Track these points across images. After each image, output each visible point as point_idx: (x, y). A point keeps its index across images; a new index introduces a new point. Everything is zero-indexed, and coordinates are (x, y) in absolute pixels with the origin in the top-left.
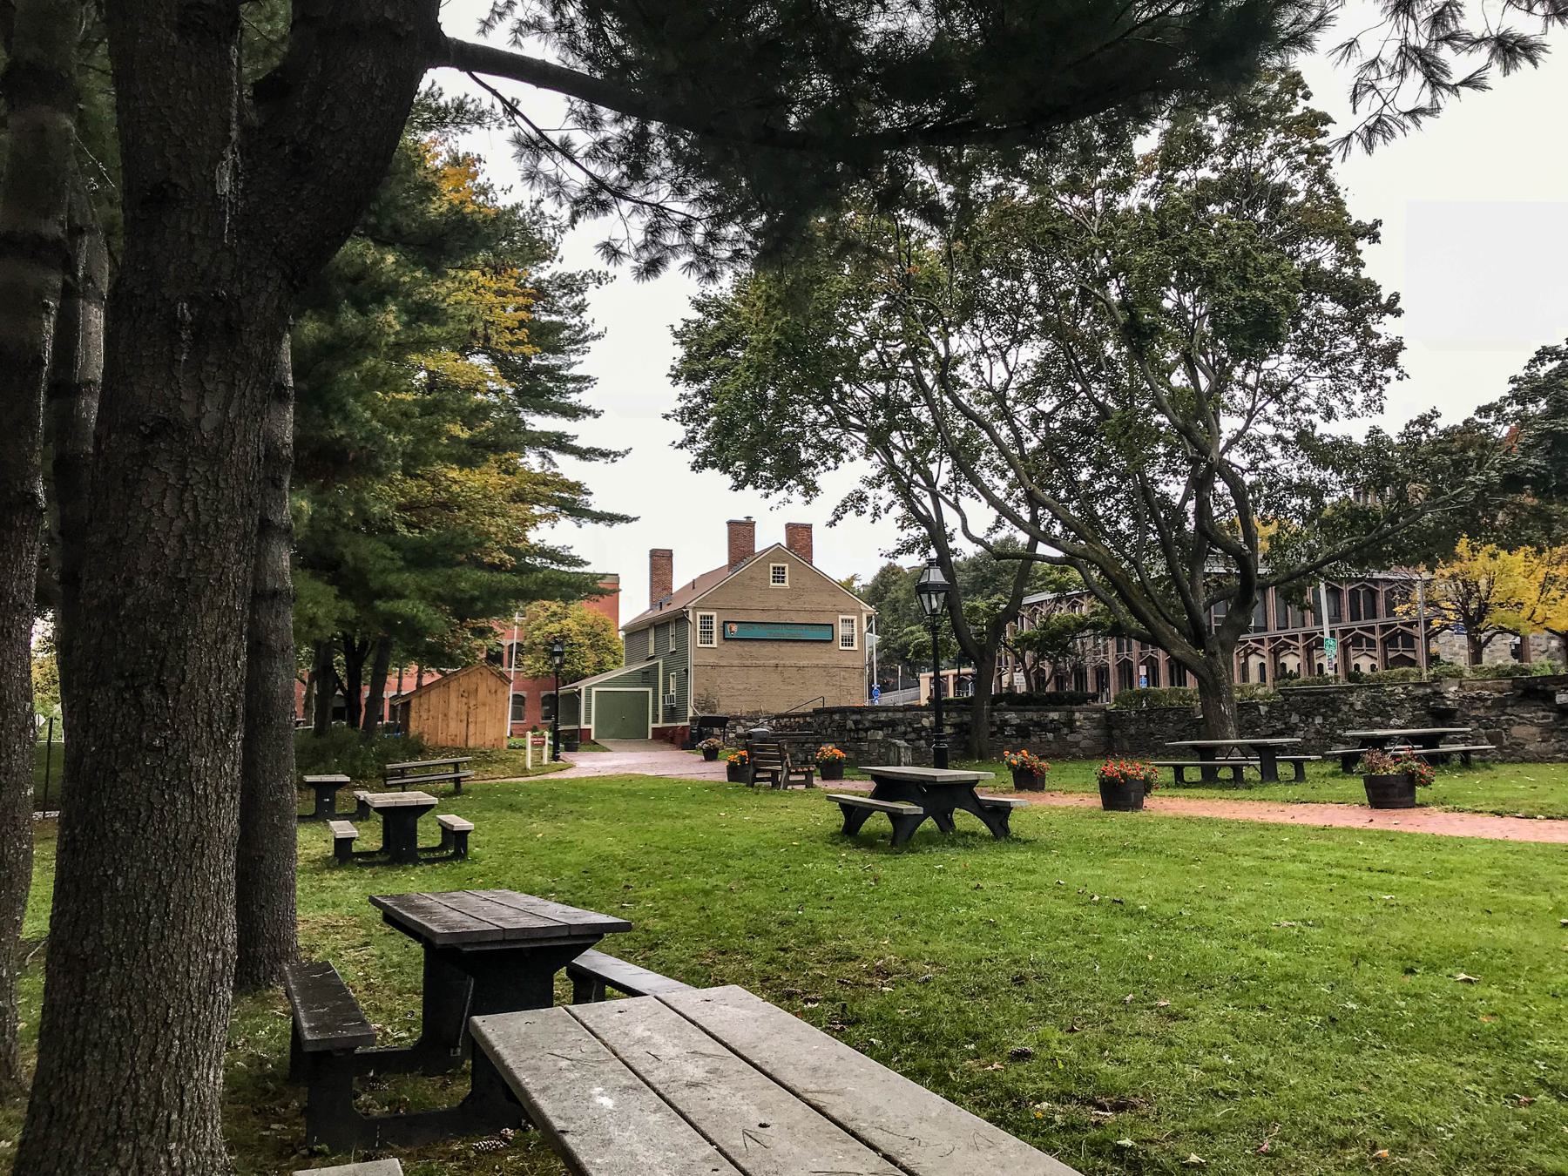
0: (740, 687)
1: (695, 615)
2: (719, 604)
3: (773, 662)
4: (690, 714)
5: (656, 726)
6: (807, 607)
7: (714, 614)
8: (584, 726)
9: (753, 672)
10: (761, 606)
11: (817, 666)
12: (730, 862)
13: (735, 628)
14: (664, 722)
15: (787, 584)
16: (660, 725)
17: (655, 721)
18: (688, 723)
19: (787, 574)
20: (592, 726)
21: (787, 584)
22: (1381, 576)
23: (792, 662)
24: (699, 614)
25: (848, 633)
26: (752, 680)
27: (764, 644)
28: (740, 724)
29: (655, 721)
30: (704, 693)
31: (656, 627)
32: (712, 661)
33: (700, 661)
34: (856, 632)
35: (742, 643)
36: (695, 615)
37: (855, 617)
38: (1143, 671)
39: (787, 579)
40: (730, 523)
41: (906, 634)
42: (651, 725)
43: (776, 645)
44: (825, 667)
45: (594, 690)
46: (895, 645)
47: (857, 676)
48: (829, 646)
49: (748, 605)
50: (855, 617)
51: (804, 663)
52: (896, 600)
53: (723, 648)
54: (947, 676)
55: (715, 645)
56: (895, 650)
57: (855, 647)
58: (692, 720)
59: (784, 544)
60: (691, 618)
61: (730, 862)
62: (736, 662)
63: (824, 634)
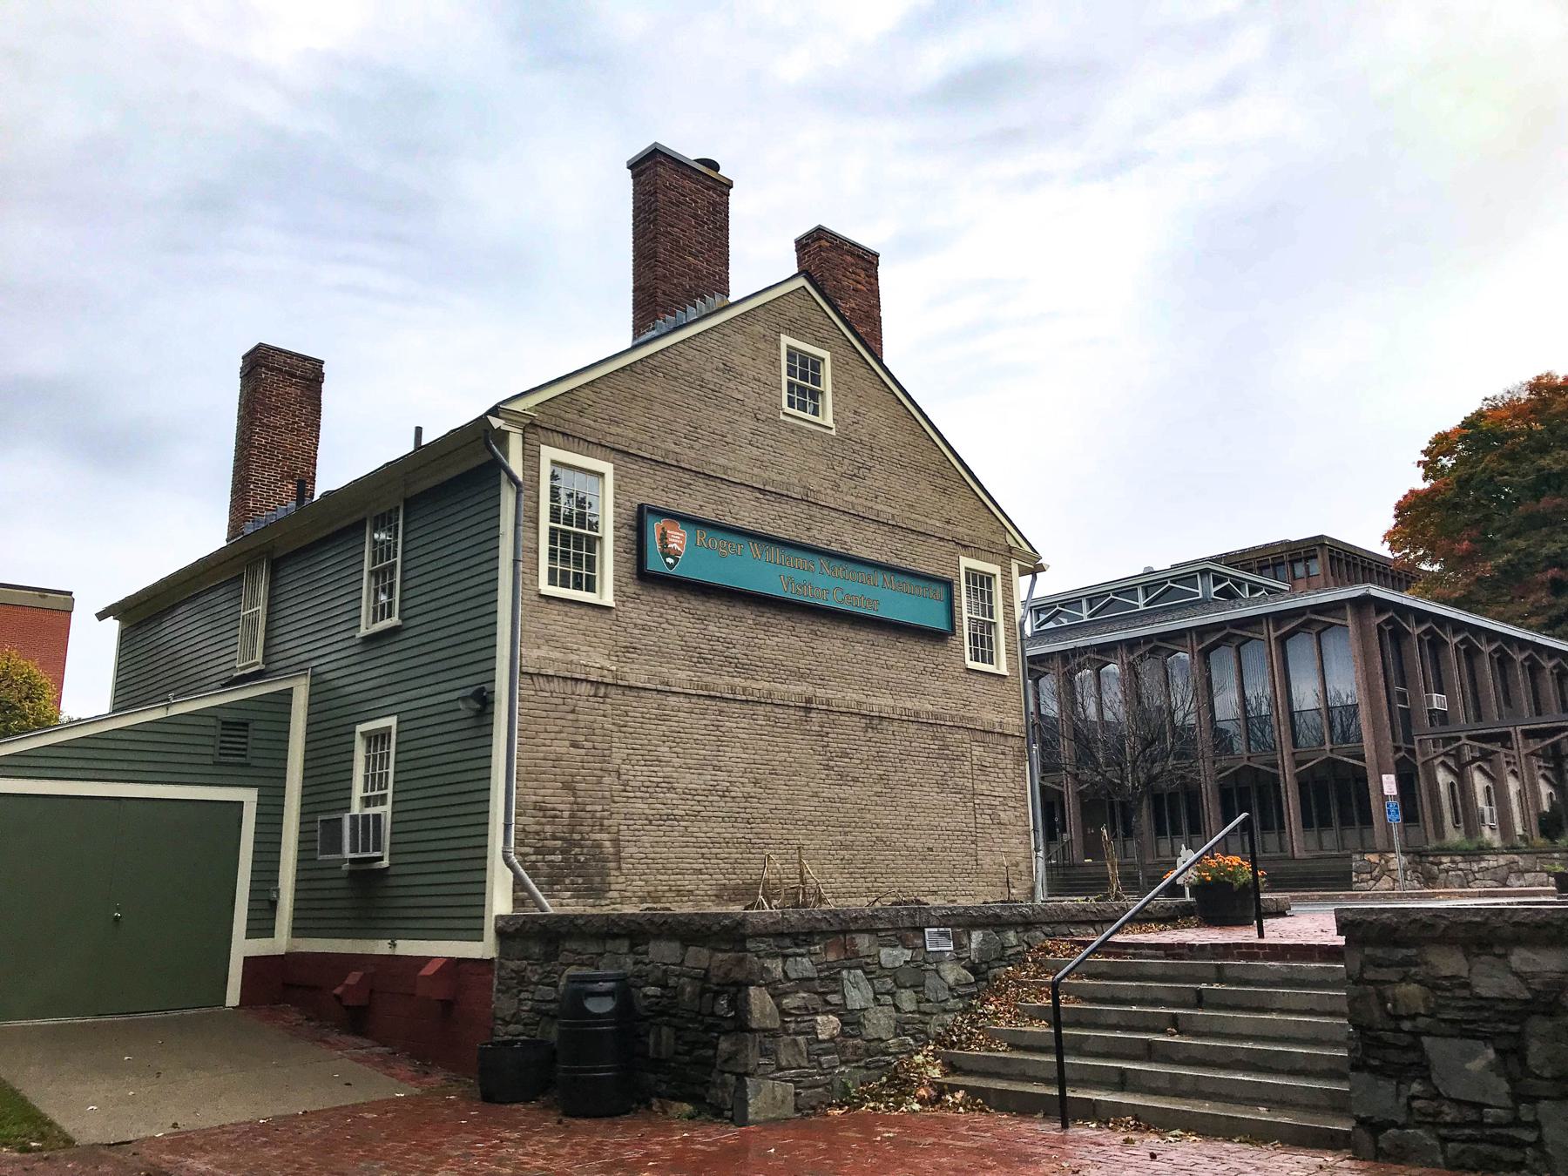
1: (531, 458)
2: (622, 434)
3: (799, 689)
4: (500, 902)
5: (261, 947)
9: (736, 723)
10: (757, 477)
11: (915, 719)
12: (779, 1097)
13: (678, 538)
14: (298, 931)
16: (281, 941)
17: (261, 924)
18: (484, 948)
19: (827, 385)
22: (1339, 727)
23: (852, 696)
24: (548, 454)
26: (732, 754)
29: (261, 924)
30: (562, 803)
31: (411, 504)
32: (596, 660)
34: (999, 617)
36: (531, 458)
38: (1390, 784)
42: (242, 947)
44: (932, 723)
48: (939, 654)
49: (719, 461)
53: (638, 613)
55: (606, 595)
58: (508, 933)
60: (515, 463)
61: (779, 1097)
62: (681, 676)
63: (921, 609)
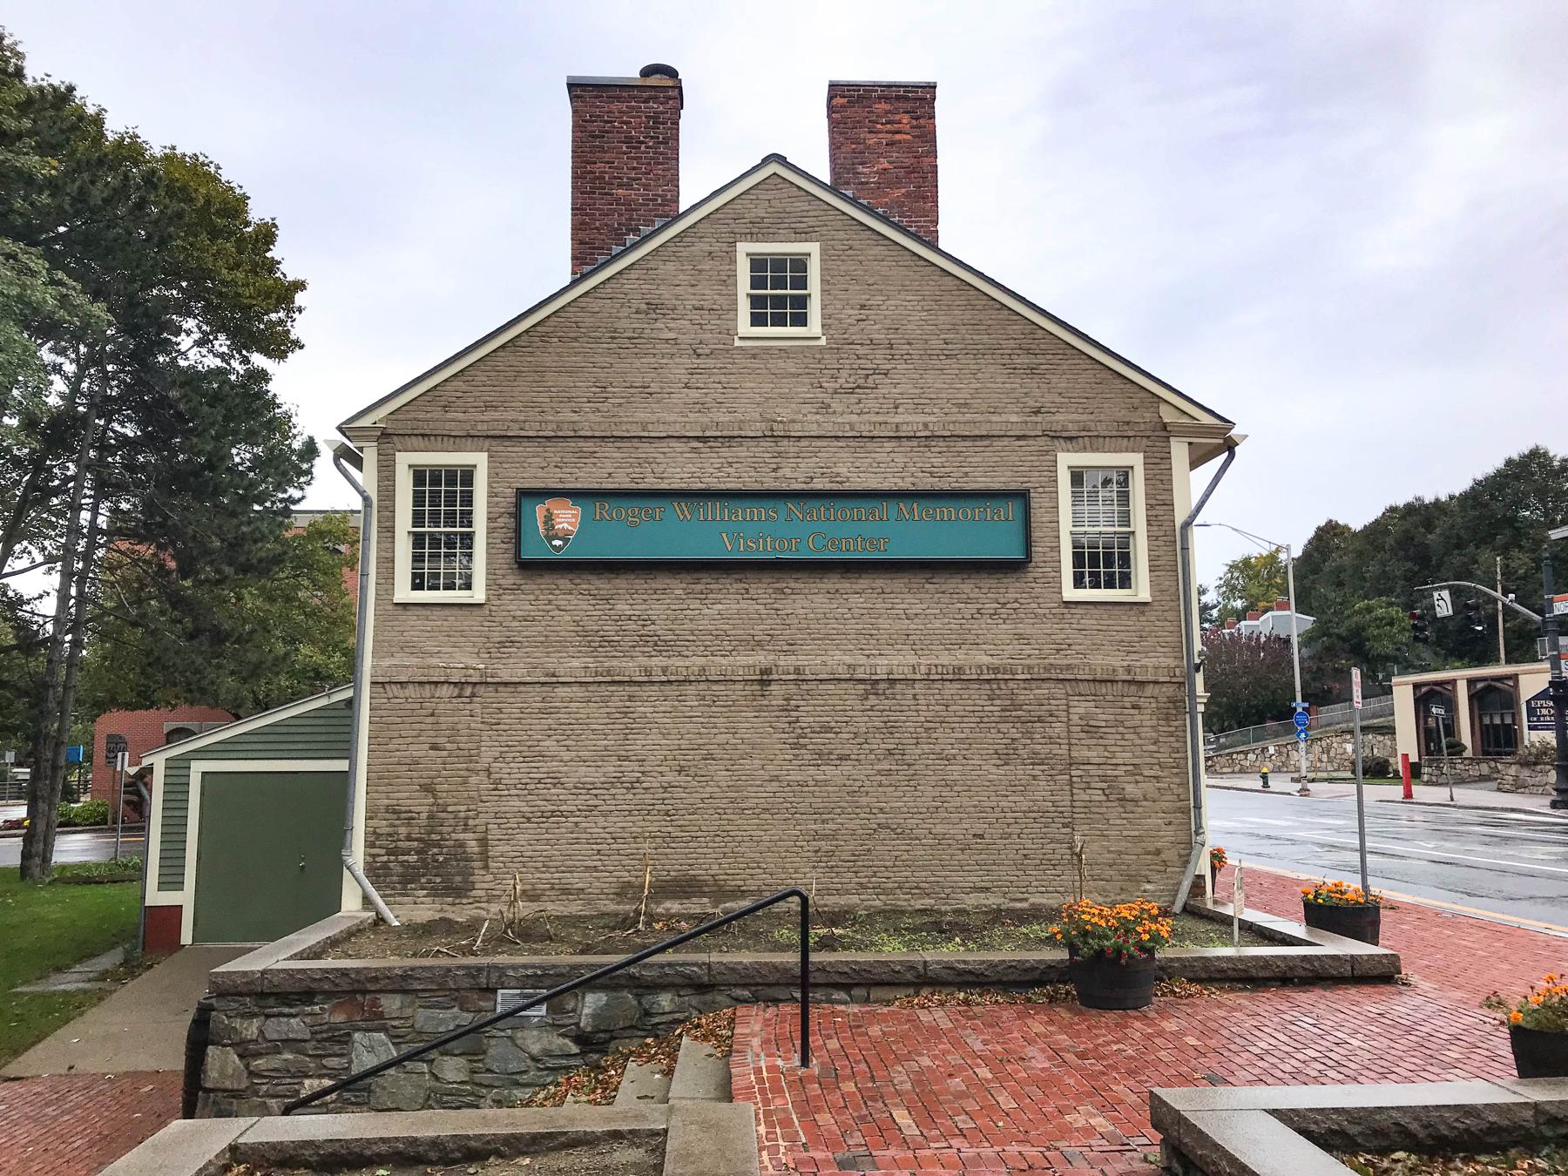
0: (583, 773)
6: (910, 420)
7: (479, 460)
8: (155, 897)
10: (695, 423)
11: (957, 675)
13: (567, 517)
15: (815, 326)
20: (184, 898)
21: (815, 326)
23: (838, 660)
24: (405, 461)
25: (1103, 527)
27: (707, 582)
28: (376, 1021)
30: (422, 806)
32: (464, 660)
33: (406, 664)
35: (601, 584)
37: (1136, 460)
39: (814, 310)
40: (577, 89)
41: (1359, 612)
43: (762, 586)
44: (992, 679)
45: (198, 768)
46: (1342, 631)
47: (1146, 720)
48: (1011, 589)
49: (639, 416)
50: (1136, 460)
51: (898, 661)
52: (1341, 569)
54: (1453, 682)
55: (478, 594)
56: (1339, 637)
57: (1142, 589)
59: (819, 164)
